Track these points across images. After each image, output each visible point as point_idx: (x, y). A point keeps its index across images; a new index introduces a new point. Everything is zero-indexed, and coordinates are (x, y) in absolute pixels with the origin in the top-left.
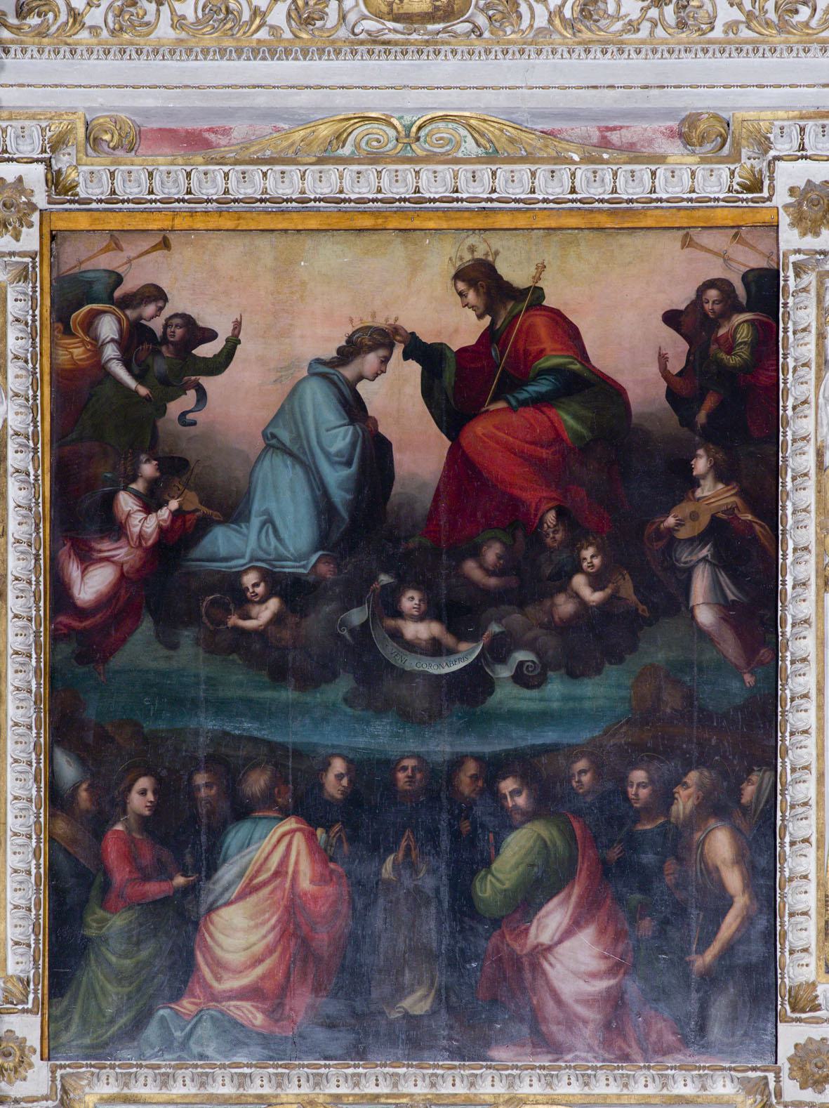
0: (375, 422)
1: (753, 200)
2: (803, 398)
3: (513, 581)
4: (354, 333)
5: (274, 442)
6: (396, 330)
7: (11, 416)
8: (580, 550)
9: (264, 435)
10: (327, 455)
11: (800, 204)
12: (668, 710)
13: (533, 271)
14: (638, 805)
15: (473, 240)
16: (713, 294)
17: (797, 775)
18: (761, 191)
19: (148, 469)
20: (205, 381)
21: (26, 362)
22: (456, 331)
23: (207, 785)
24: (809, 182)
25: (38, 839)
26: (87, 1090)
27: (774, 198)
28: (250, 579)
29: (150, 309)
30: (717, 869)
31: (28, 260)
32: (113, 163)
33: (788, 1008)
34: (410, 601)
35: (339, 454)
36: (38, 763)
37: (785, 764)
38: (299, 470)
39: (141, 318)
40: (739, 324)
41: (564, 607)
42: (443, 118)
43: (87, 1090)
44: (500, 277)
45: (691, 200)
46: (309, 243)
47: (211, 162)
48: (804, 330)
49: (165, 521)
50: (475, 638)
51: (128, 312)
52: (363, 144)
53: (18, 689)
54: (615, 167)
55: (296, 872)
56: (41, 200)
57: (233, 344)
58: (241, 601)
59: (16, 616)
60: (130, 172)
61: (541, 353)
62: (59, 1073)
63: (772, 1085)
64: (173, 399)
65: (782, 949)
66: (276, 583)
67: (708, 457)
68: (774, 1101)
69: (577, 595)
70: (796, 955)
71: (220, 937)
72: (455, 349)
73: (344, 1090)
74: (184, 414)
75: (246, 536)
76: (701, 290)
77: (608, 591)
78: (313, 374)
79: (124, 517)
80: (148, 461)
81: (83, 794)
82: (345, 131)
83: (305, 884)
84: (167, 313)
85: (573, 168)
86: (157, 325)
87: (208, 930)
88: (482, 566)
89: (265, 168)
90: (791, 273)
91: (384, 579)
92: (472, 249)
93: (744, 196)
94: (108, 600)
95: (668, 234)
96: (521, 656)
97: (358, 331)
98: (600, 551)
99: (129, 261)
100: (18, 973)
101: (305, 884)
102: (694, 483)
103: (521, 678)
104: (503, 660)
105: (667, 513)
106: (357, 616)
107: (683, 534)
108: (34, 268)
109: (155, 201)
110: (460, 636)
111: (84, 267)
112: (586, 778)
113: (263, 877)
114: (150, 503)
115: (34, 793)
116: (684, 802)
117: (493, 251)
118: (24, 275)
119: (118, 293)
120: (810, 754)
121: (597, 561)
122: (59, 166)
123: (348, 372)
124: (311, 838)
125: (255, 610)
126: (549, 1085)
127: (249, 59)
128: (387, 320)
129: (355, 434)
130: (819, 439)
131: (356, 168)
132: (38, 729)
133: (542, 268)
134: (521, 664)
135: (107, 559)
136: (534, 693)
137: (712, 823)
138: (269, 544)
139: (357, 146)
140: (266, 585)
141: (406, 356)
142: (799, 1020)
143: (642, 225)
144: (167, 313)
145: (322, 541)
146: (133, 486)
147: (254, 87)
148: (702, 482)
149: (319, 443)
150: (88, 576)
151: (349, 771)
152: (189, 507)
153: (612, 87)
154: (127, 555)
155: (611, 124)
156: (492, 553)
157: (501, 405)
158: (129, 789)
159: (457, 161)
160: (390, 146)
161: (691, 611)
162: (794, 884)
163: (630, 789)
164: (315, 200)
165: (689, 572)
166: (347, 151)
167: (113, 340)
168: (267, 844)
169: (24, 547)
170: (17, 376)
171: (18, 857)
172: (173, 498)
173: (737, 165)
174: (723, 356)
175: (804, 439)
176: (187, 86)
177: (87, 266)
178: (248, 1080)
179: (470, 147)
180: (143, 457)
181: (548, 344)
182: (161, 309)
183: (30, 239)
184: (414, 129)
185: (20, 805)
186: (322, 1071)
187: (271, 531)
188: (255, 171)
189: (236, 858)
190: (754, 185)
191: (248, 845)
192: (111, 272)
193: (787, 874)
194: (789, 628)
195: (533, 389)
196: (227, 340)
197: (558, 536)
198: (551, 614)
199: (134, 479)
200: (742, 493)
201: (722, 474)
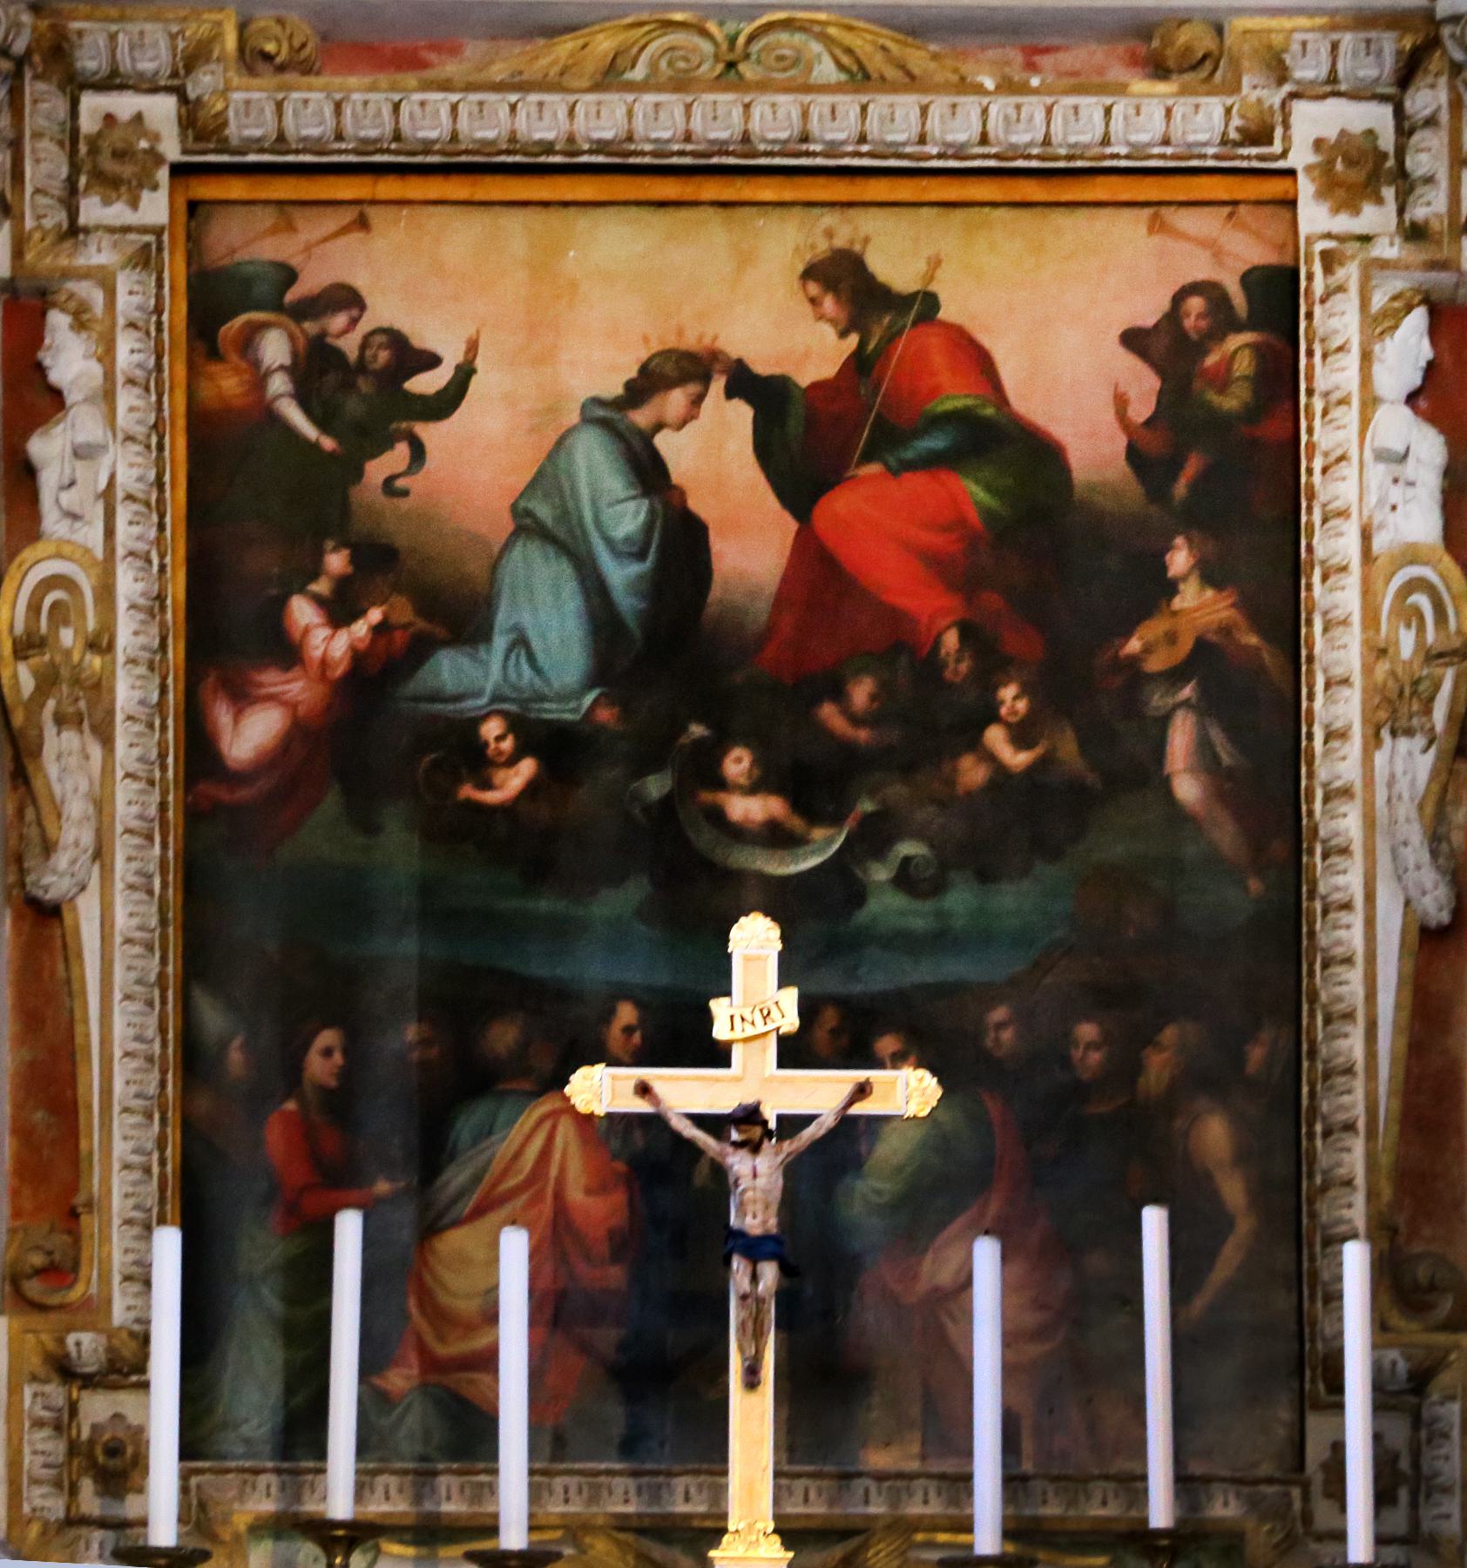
0: (682, 493)
2: (1339, 452)
3: (893, 735)
4: (650, 359)
5: (528, 521)
6: (714, 355)
8: (996, 688)
9: (514, 508)
10: (609, 542)
11: (1330, 163)
12: (1131, 934)
13: (922, 266)
15: (829, 219)
16: (1195, 304)
18: (1270, 142)
19: (337, 562)
22: (807, 355)
25: (163, 1121)
27: (1291, 155)
28: (492, 729)
29: (339, 321)
30: (1208, 1176)
32: (280, 88)
33: (1321, 1387)
35: (627, 540)
38: (565, 569)
39: (323, 335)
40: (1236, 352)
42: (787, 25)
43: (236, 1506)
47: (427, 86)
49: (360, 640)
50: (836, 820)
51: (307, 325)
52: (663, 64)
54: (1049, 100)
55: (562, 1170)
56: (172, 150)
57: (465, 374)
58: (479, 764)
60: (306, 102)
61: (934, 392)
62: (194, 1481)
63: (1297, 1505)
64: (374, 455)
67: (1191, 548)
69: (991, 758)
71: (448, 1277)
75: (485, 665)
78: (587, 420)
80: (335, 549)
81: (236, 1057)
82: (634, 43)
84: (364, 326)
85: (985, 101)
86: (350, 345)
89: (513, 98)
90: (1318, 268)
91: (697, 730)
92: (829, 234)
95: (1127, 213)
96: (908, 848)
99: (308, 249)
100: (129, 1324)
101: (576, 1194)
103: (905, 879)
105: (1128, 635)
106: (656, 786)
107: (1155, 664)
109: (346, 151)
110: (813, 816)
111: (238, 257)
112: (1007, 1035)
113: (511, 1182)
114: (340, 611)
116: (1158, 1068)
117: (862, 235)
118: (145, 259)
119: (290, 297)
121: (1022, 705)
122: (199, 91)
123: (641, 417)
125: (499, 775)
128: (700, 339)
129: (652, 512)
130: (1366, 513)
133: (935, 263)
134: (907, 860)
135: (271, 698)
136: (927, 906)
137: (1202, 1103)
138: (520, 675)
139: (653, 66)
140: (517, 738)
141: (730, 393)
144: (364, 326)
145: (602, 673)
148: (1182, 587)
150: (242, 723)
151: (642, 1022)
154: (303, 690)
156: (861, 693)
157: (874, 468)
158: (306, 1046)
159: (808, 89)
160: (705, 67)
163: (1073, 1052)
165: (1164, 721)
166: (638, 73)
167: (282, 367)
172: (373, 604)
174: (1213, 397)
178: (486, 1490)
179: (826, 70)
180: (330, 544)
181: (945, 378)
182: (354, 322)
183: (156, 207)
184: (741, 40)
187: (523, 660)
188: (498, 103)
189: (470, 1153)
190: (1258, 135)
191: (490, 1133)
196: (458, 368)
197: (964, 667)
198: (951, 782)
201: (1210, 574)
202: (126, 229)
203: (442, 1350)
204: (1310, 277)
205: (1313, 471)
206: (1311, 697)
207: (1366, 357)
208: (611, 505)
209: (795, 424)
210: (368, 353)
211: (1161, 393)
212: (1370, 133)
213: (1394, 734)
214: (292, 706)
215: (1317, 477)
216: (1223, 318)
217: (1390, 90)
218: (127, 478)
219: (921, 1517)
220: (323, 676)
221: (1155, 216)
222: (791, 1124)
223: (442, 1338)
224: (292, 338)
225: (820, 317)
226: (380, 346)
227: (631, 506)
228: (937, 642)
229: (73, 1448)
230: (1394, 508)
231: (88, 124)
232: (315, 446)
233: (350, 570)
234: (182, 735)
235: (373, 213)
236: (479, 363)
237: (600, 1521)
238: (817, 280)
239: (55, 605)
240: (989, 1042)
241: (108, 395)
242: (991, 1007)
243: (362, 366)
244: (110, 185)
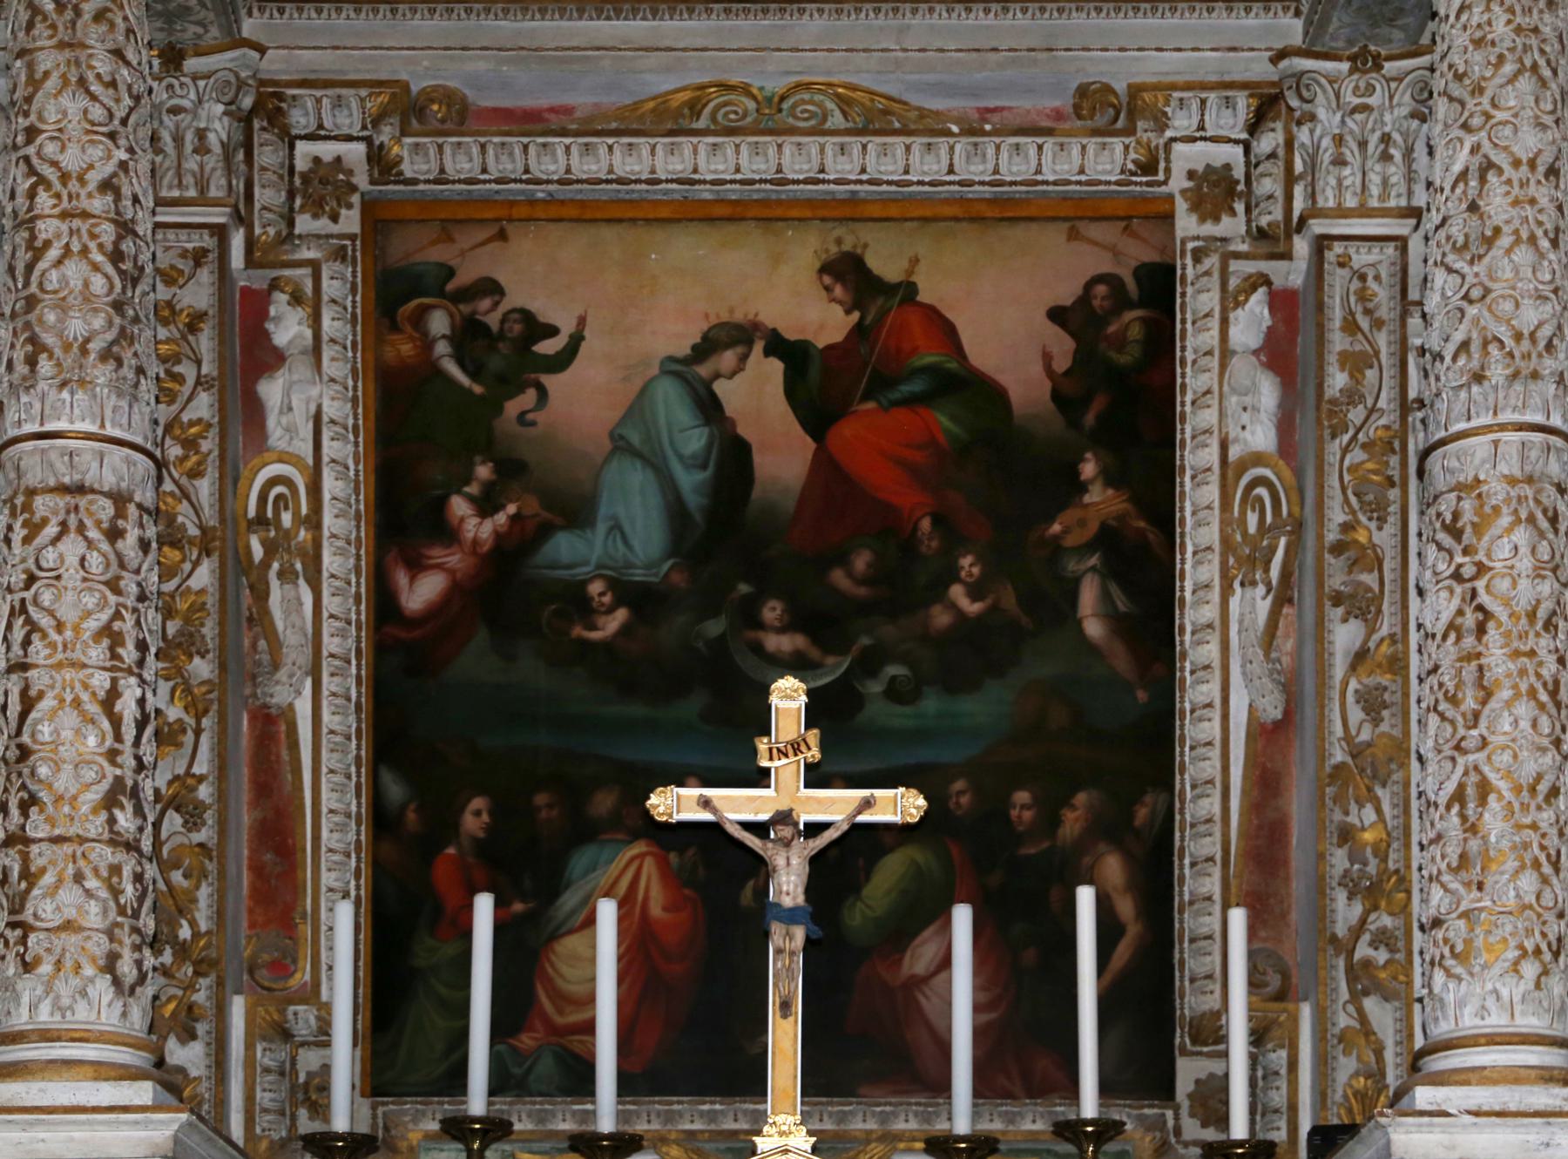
0: (733, 423)
1: (1148, 184)
4: (710, 329)
5: (621, 443)
7: (326, 403)
9: (612, 435)
10: (681, 457)
11: (1199, 188)
13: (905, 264)
14: (1021, 828)
15: (840, 231)
16: (1101, 289)
17: (1198, 791)
18: (1156, 173)
19: (484, 471)
20: (548, 380)
21: (345, 348)
23: (550, 806)
24: (1208, 166)
26: (411, 1126)
27: (1171, 182)
28: (595, 588)
29: (485, 304)
31: (348, 243)
33: (1187, 1041)
34: (772, 611)
35: (694, 456)
36: (359, 776)
37: (1184, 782)
38: (650, 475)
39: (474, 313)
41: (941, 618)
43: (411, 1126)
44: (869, 272)
45: (1079, 183)
46: (658, 234)
48: (1207, 316)
50: (842, 650)
51: (462, 307)
52: (720, 117)
53: (334, 694)
56: (361, 180)
57: (576, 341)
58: (585, 610)
59: (332, 616)
61: (914, 351)
63: (1171, 1123)
64: (511, 397)
65: (1182, 977)
66: (627, 592)
67: (1098, 459)
68: (1173, 1140)
69: (953, 606)
70: (1198, 984)
71: (565, 969)
72: (820, 345)
73: (697, 1126)
74: (523, 413)
76: (1089, 285)
77: (989, 601)
78: (665, 372)
79: (456, 522)
80: (484, 462)
81: (411, 816)
83: (656, 910)
84: (505, 306)
85: (952, 140)
86: (493, 320)
87: (549, 960)
88: (850, 575)
89: (610, 141)
90: (1189, 261)
91: (744, 588)
92: (839, 241)
93: (1138, 179)
94: (435, 611)
96: (893, 670)
97: (715, 326)
98: (980, 559)
101: (656, 910)
102: (1082, 488)
103: (894, 693)
104: (873, 673)
105: (1051, 519)
106: (714, 627)
107: (1070, 541)
108: (354, 250)
109: (489, 181)
110: (828, 650)
114: (486, 505)
115: (354, 808)
116: (1072, 822)
119: (450, 287)
120: (1214, 767)
121: (976, 570)
123: (704, 370)
124: (663, 864)
125: (601, 620)
126: (928, 1121)
127: (591, 19)
129: (711, 436)
131: (711, 140)
132: (359, 738)
133: (915, 261)
134: (893, 679)
135: (439, 567)
136: (907, 710)
137: (1102, 847)
140: (614, 594)
141: (768, 352)
142: (1200, 1054)
143: (1024, 214)
144: (505, 306)
146: (467, 489)
147: (598, 49)
149: (672, 443)
152: (527, 512)
153: (995, 50)
155: (992, 104)
156: (861, 562)
157: (871, 405)
158: (462, 810)
161: (1079, 623)
162: (1196, 907)
164: (667, 181)
165: (1077, 581)
166: (702, 124)
167: (444, 337)
168: (614, 869)
169: (340, 543)
170: (333, 359)
171: (333, 875)
172: (511, 501)
173: (1132, 139)
174: (1113, 355)
175: (1205, 432)
176: (522, 48)
177: (418, 258)
180: (478, 459)
182: (496, 304)
183: (351, 221)
185: (337, 819)
186: (676, 1107)
190: (1148, 167)
191: (594, 869)
192: (441, 265)
193: (1187, 898)
194: (1188, 637)
195: (906, 389)
196: (571, 336)
197: (934, 544)
199: (467, 482)
200: (1135, 499)
201: (1111, 478)
202: (329, 236)
203: (560, 1020)
204: (1184, 268)
205: (1185, 402)
206: (1183, 561)
207: (1225, 323)
208: (682, 431)
209: (814, 372)
210: (507, 326)
211: (1076, 352)
212: (1228, 167)
213: (1242, 584)
214: (451, 572)
215: (1188, 408)
216: (1120, 299)
217: (1244, 136)
218: (331, 409)
219: (904, 1131)
220: (474, 552)
221: (1072, 228)
222: (814, 829)
223: (561, 1012)
224: (451, 316)
225: (833, 300)
226: (515, 321)
227: (697, 431)
228: (915, 528)
229: (294, 1088)
230: (1244, 428)
231: (301, 165)
232: (469, 392)
233: (494, 477)
234: (372, 618)
235: (510, 229)
236: (587, 333)
237: (673, 1136)
238: (829, 274)
239: (279, 497)
240: (952, 805)
241: (317, 350)
242: (952, 781)
243: (501, 335)
244: (316, 207)
